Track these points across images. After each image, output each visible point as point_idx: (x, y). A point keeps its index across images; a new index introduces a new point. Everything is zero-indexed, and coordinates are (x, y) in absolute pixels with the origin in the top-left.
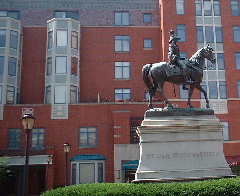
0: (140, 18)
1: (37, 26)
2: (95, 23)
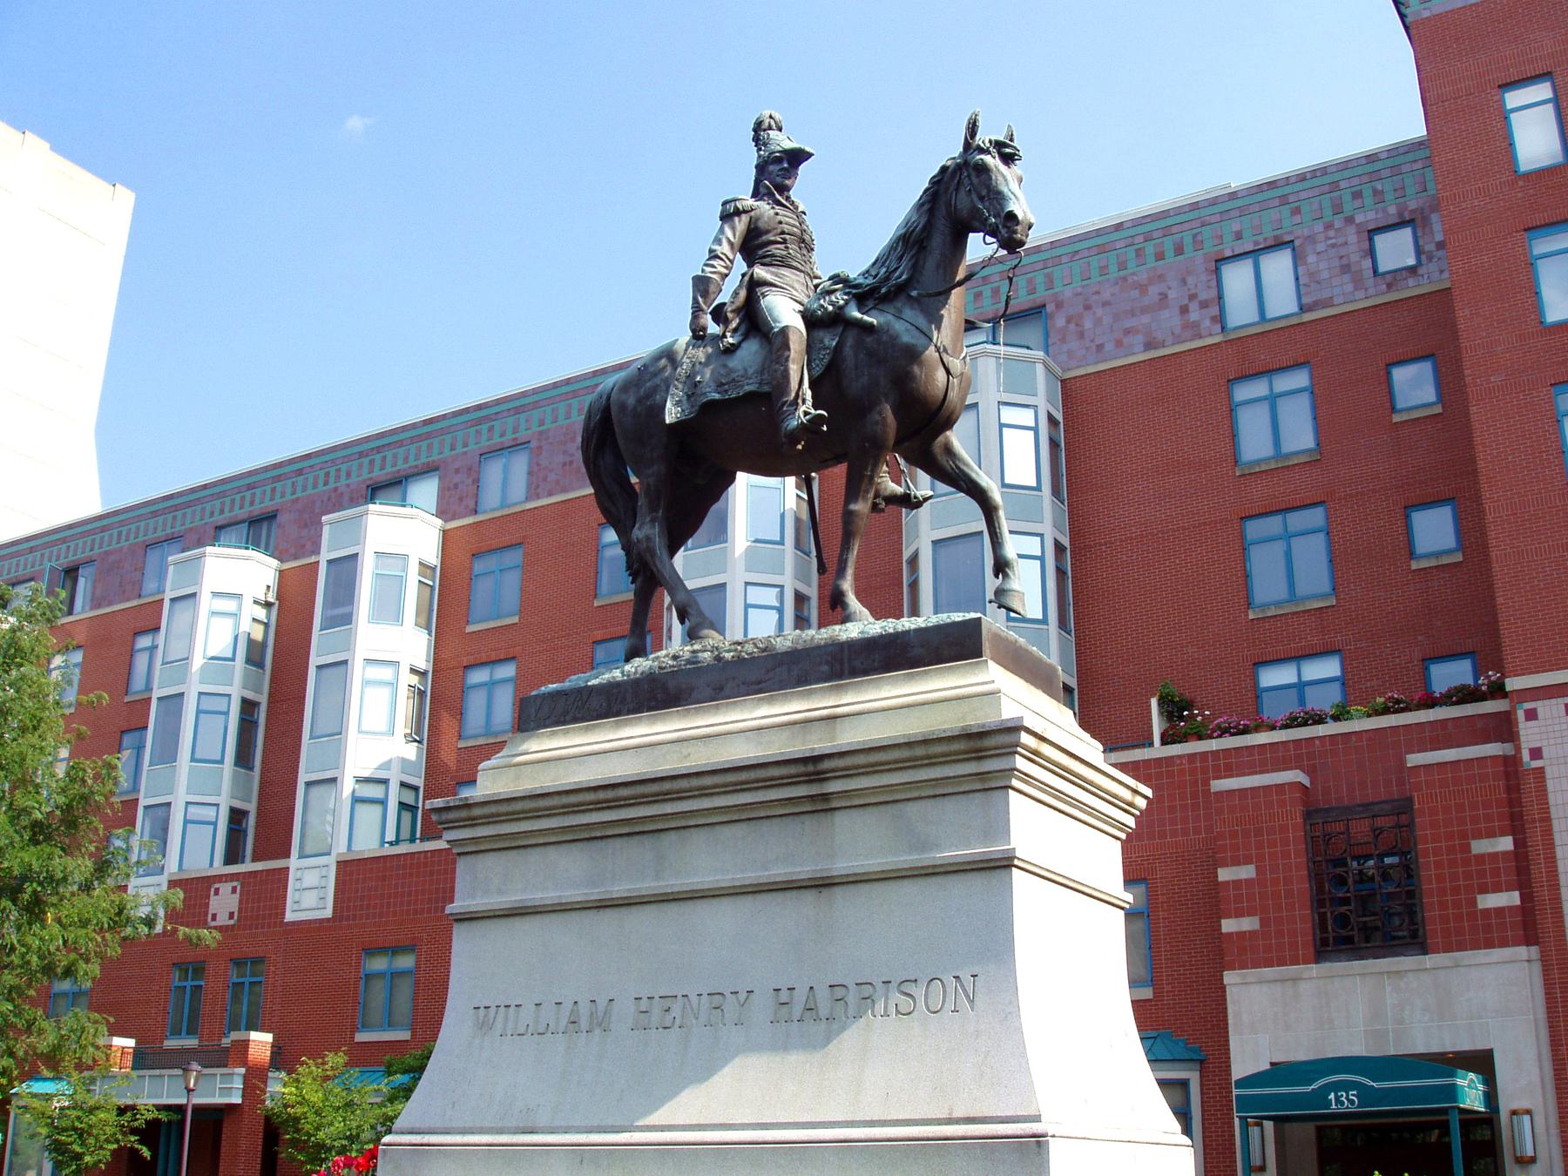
0: (1354, 258)
2: (1126, 341)
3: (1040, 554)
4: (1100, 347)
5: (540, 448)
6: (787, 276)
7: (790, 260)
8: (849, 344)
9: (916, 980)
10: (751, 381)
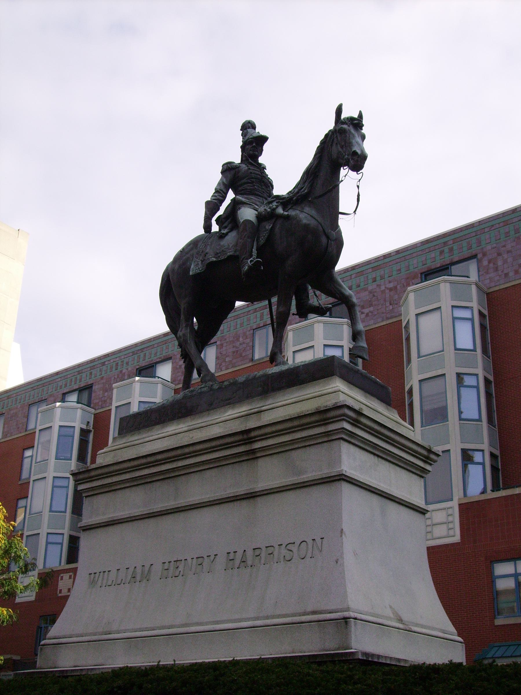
1: (390, 321)
3: (476, 385)
4: (506, 275)
5: (222, 345)
6: (253, 199)
7: (255, 191)
8: (278, 227)
9: (294, 543)
10: (231, 251)
